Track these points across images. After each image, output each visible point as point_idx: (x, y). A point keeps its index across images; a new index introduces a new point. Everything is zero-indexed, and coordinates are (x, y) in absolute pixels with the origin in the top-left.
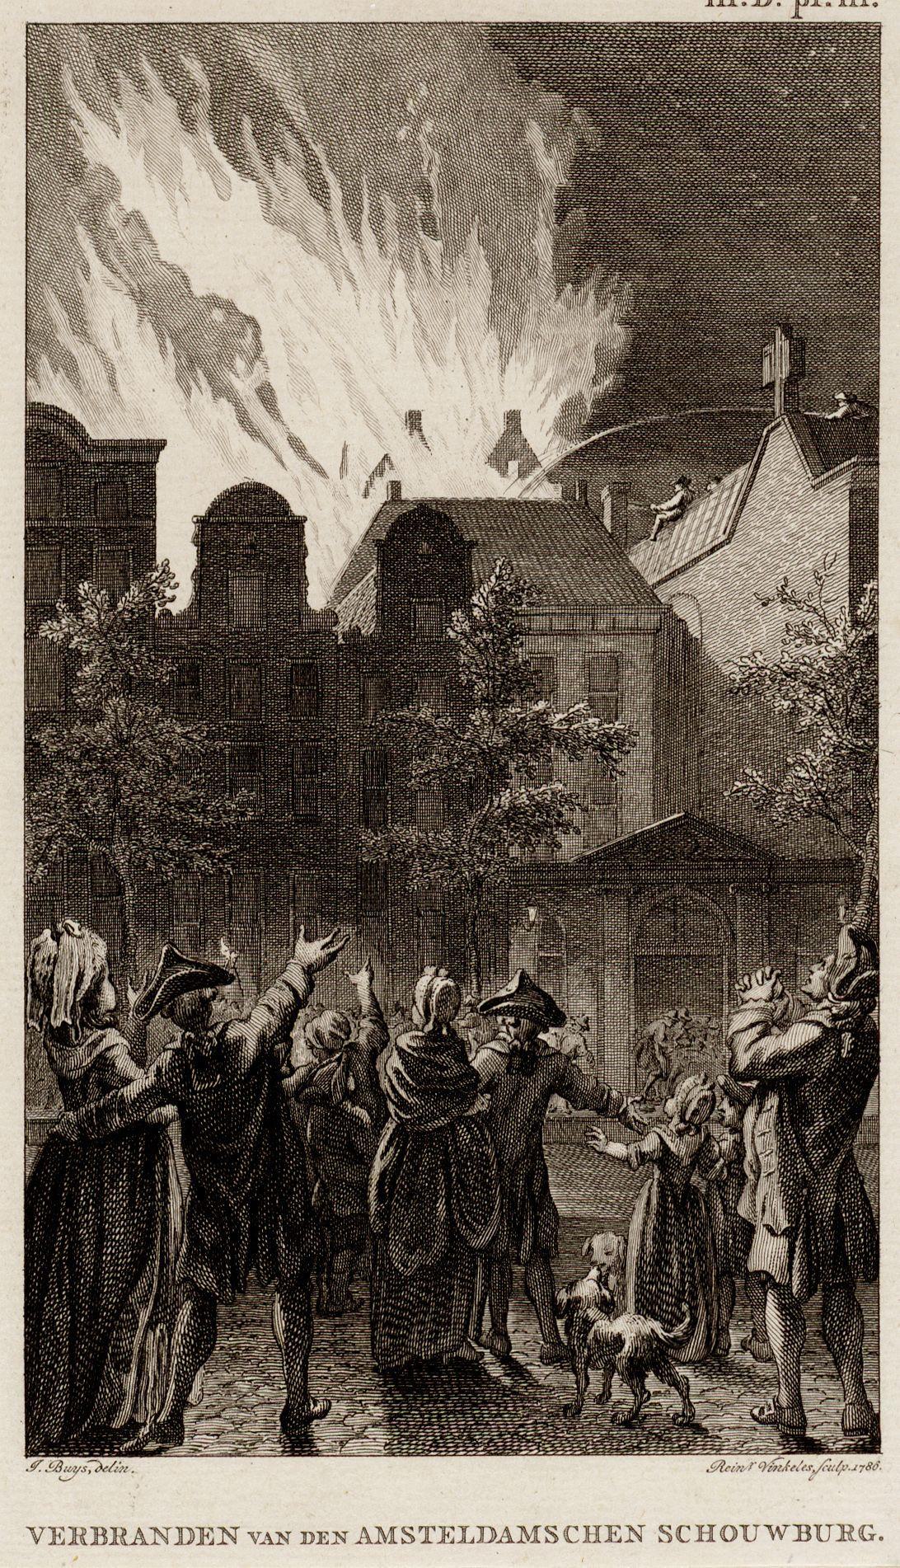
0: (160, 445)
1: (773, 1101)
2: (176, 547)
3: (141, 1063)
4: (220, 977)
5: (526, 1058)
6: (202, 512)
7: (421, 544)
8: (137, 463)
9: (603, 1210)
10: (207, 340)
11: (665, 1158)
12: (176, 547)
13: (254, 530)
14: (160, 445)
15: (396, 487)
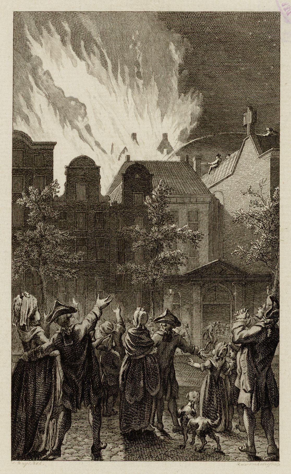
0: (54, 144)
1: (246, 350)
2: (59, 176)
4: (73, 310)
5: (168, 337)
6: (68, 165)
7: (136, 175)
8: (48, 149)
10: (68, 109)
11: (212, 368)
12: (59, 176)
13: (84, 171)
14: (54, 144)
15: (128, 157)
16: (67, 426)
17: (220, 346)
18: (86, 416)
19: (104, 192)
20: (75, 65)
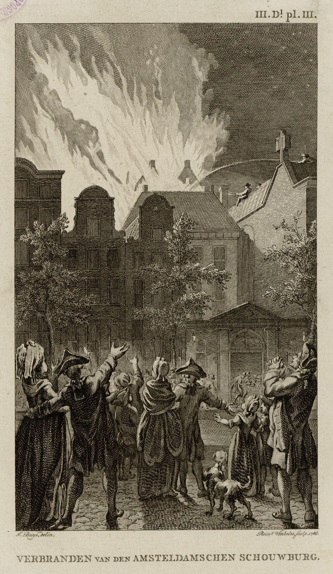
1: (280, 404)
2: (68, 208)
3: (56, 391)
7: (154, 207)
9: (219, 440)
10: (78, 135)
11: (241, 424)
12: (68, 208)
13: (96, 202)
15: (146, 187)
16: (78, 492)
17: (250, 400)
18: (98, 480)
19: (118, 226)
20: (85, 84)
